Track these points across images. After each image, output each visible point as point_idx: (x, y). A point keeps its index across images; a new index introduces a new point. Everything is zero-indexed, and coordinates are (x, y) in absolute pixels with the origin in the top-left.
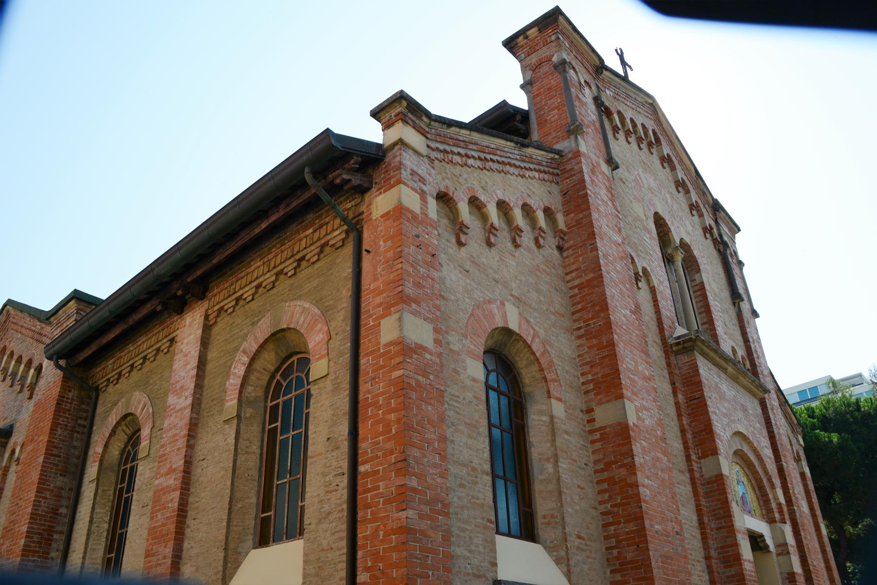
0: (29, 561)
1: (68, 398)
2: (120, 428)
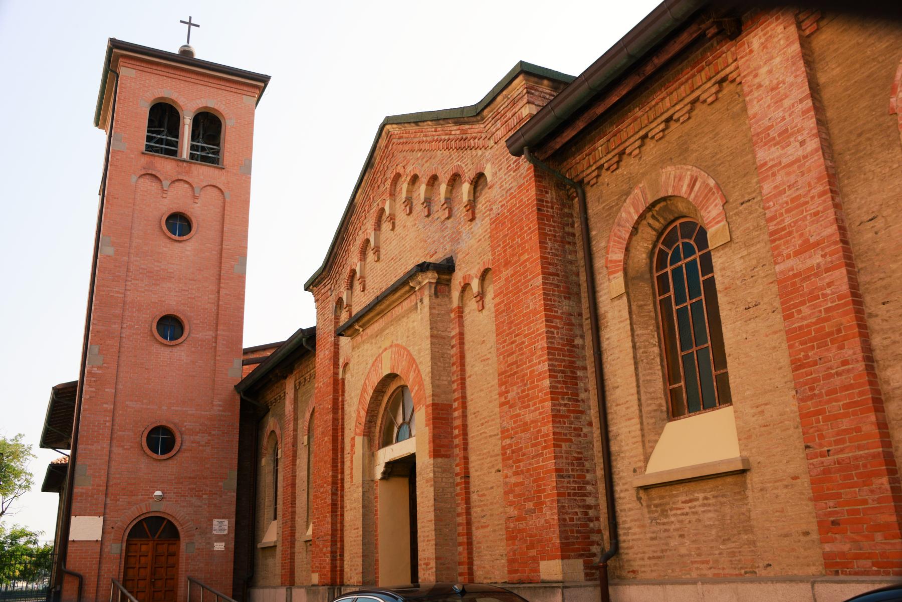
0: (561, 405)
1: (547, 202)
2: (644, 222)
